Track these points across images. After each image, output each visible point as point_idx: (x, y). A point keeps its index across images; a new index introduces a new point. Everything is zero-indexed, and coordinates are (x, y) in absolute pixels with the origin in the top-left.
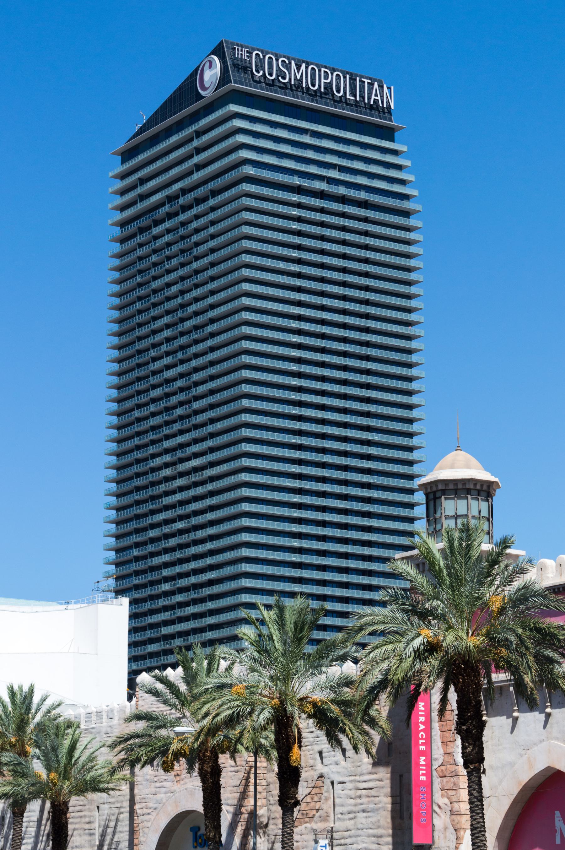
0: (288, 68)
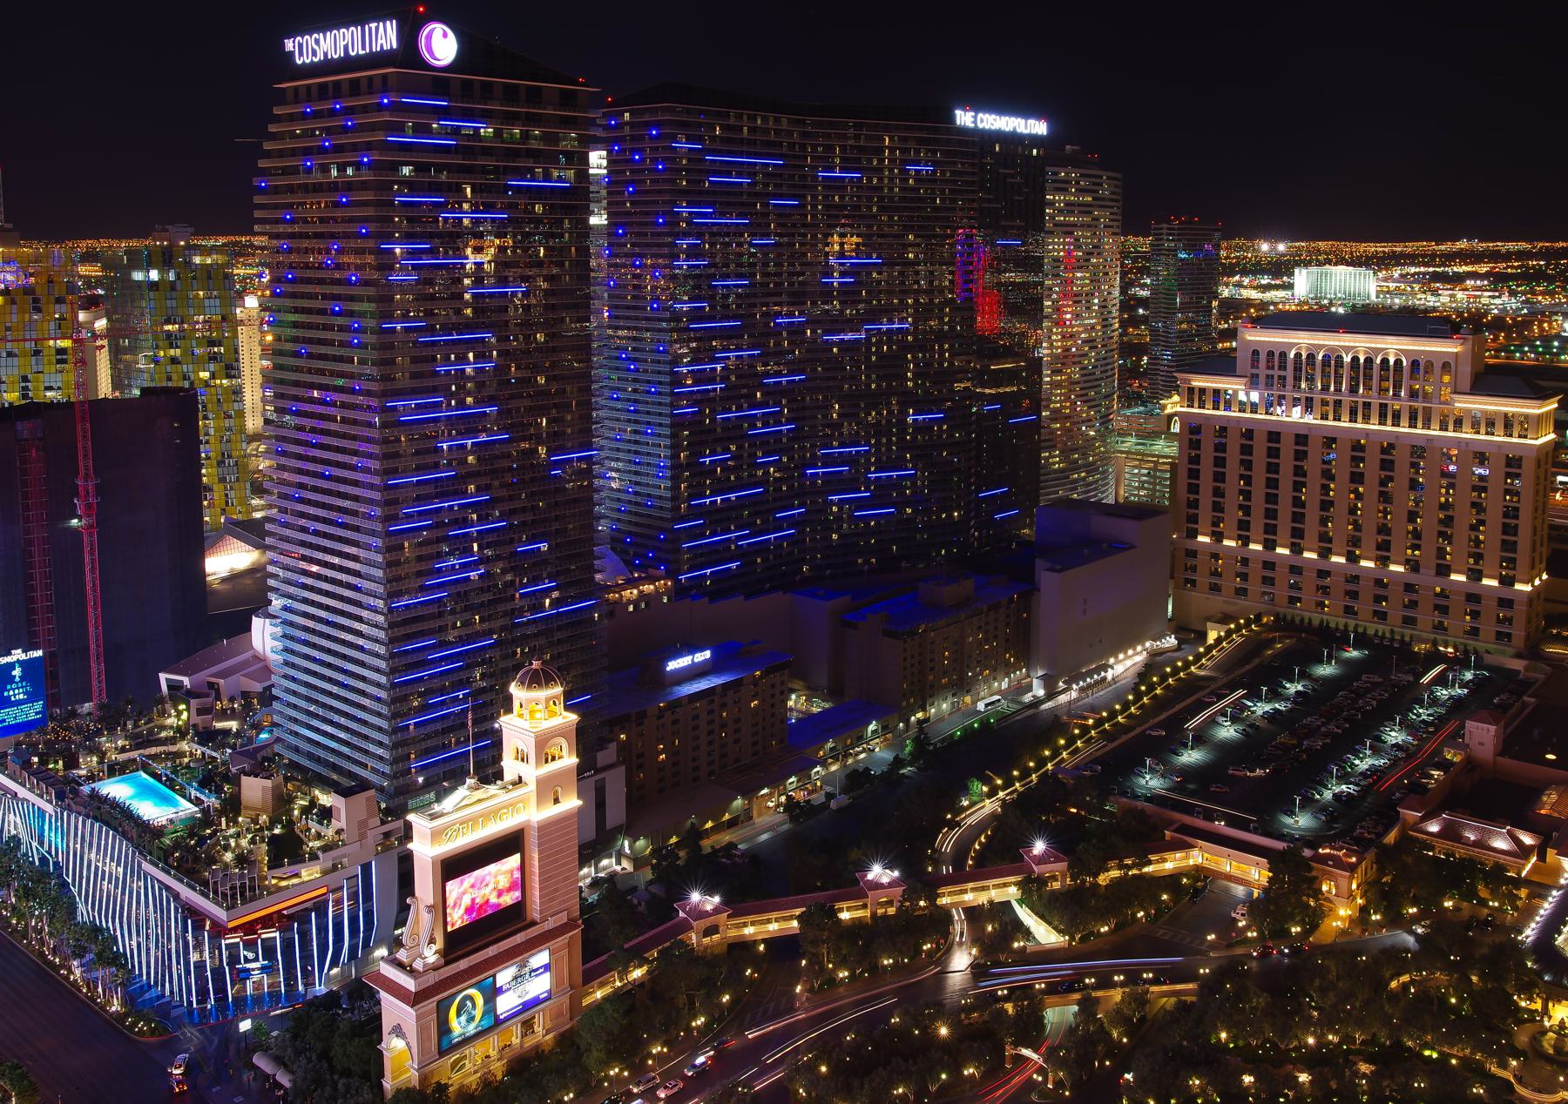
0: (317, 42)
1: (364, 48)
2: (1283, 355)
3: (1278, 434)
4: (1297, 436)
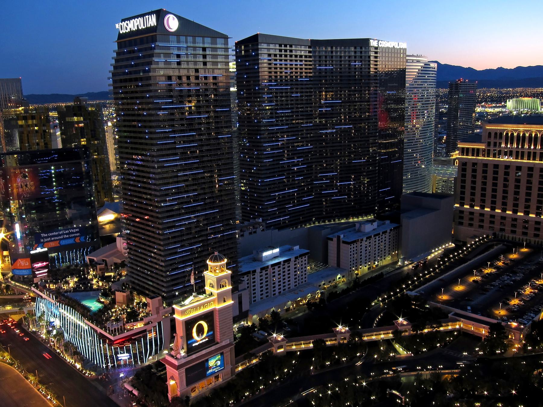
0: (127, 24)
1: (144, 26)
2: (501, 134)
3: (498, 165)
4: (494, 165)
